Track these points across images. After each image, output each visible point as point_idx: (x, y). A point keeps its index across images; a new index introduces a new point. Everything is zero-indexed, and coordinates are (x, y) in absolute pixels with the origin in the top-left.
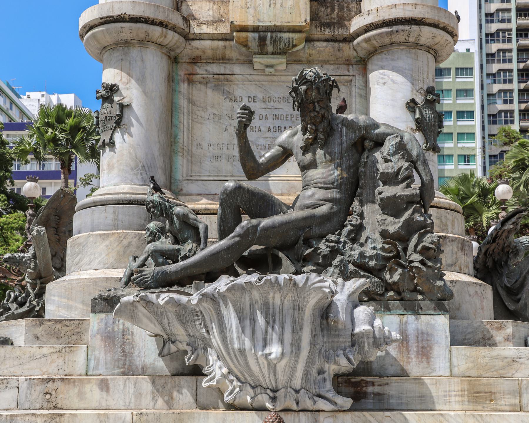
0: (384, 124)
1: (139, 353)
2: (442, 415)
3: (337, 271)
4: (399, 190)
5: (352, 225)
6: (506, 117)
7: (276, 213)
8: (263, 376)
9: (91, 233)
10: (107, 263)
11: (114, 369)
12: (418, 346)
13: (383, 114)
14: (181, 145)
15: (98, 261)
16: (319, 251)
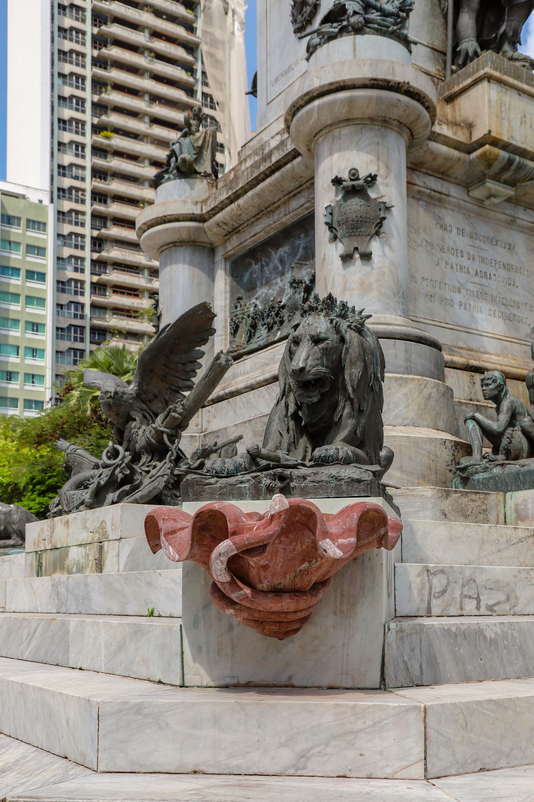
6: (76, 287)
15: (394, 414)
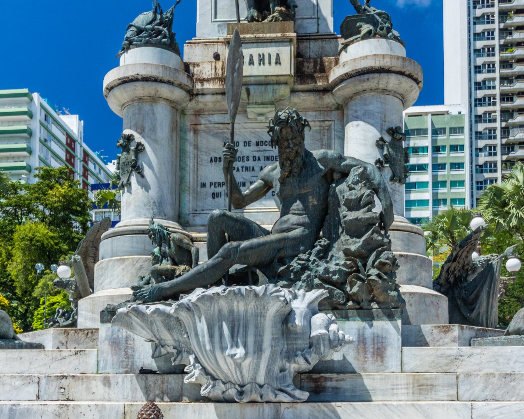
0: (350, 158)
1: (140, 355)
2: (386, 405)
3: (304, 284)
4: (360, 214)
5: (321, 246)
7: (257, 236)
8: (232, 374)
9: (111, 258)
10: (123, 283)
11: (119, 368)
12: (374, 348)
13: (357, 151)
14: (187, 185)
16: (291, 268)
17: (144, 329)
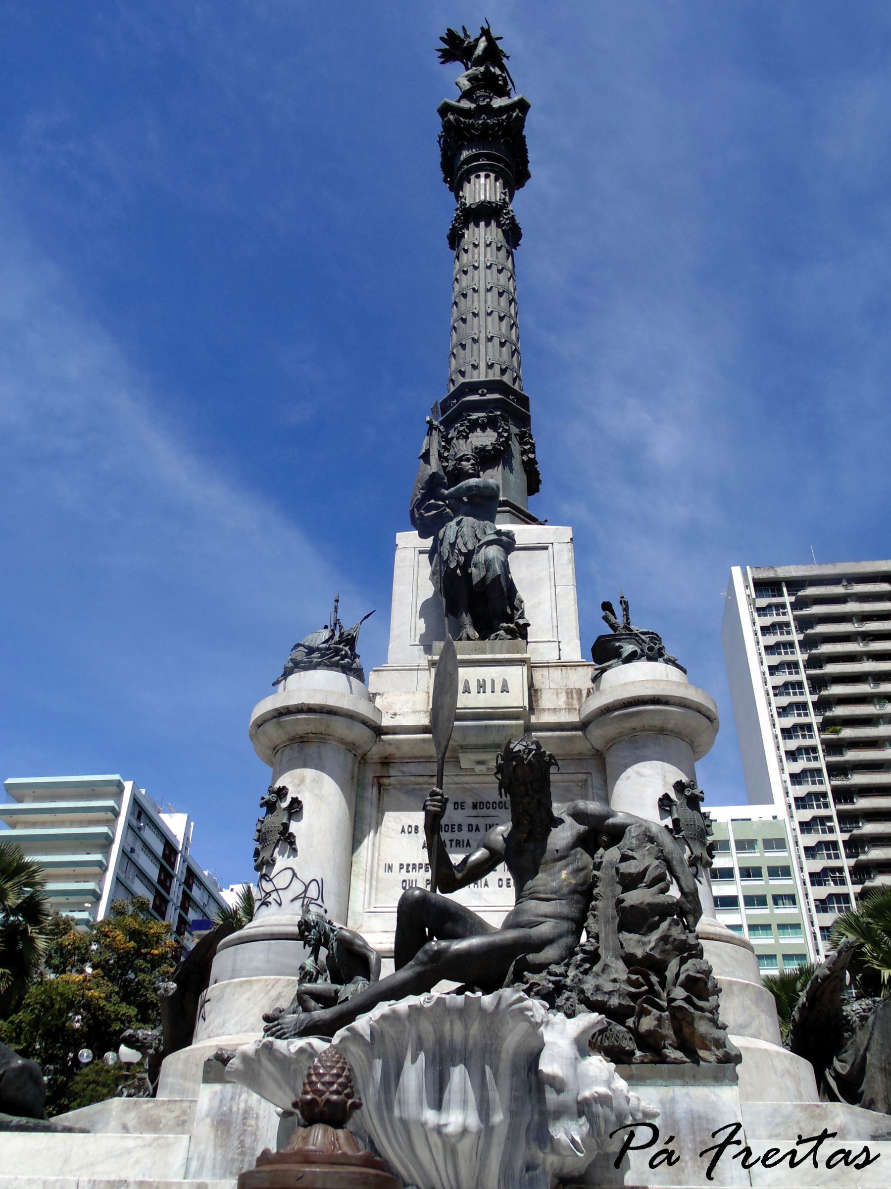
8: (437, 1170)
9: (231, 981)
12: (694, 1140)
17: (280, 1087)
